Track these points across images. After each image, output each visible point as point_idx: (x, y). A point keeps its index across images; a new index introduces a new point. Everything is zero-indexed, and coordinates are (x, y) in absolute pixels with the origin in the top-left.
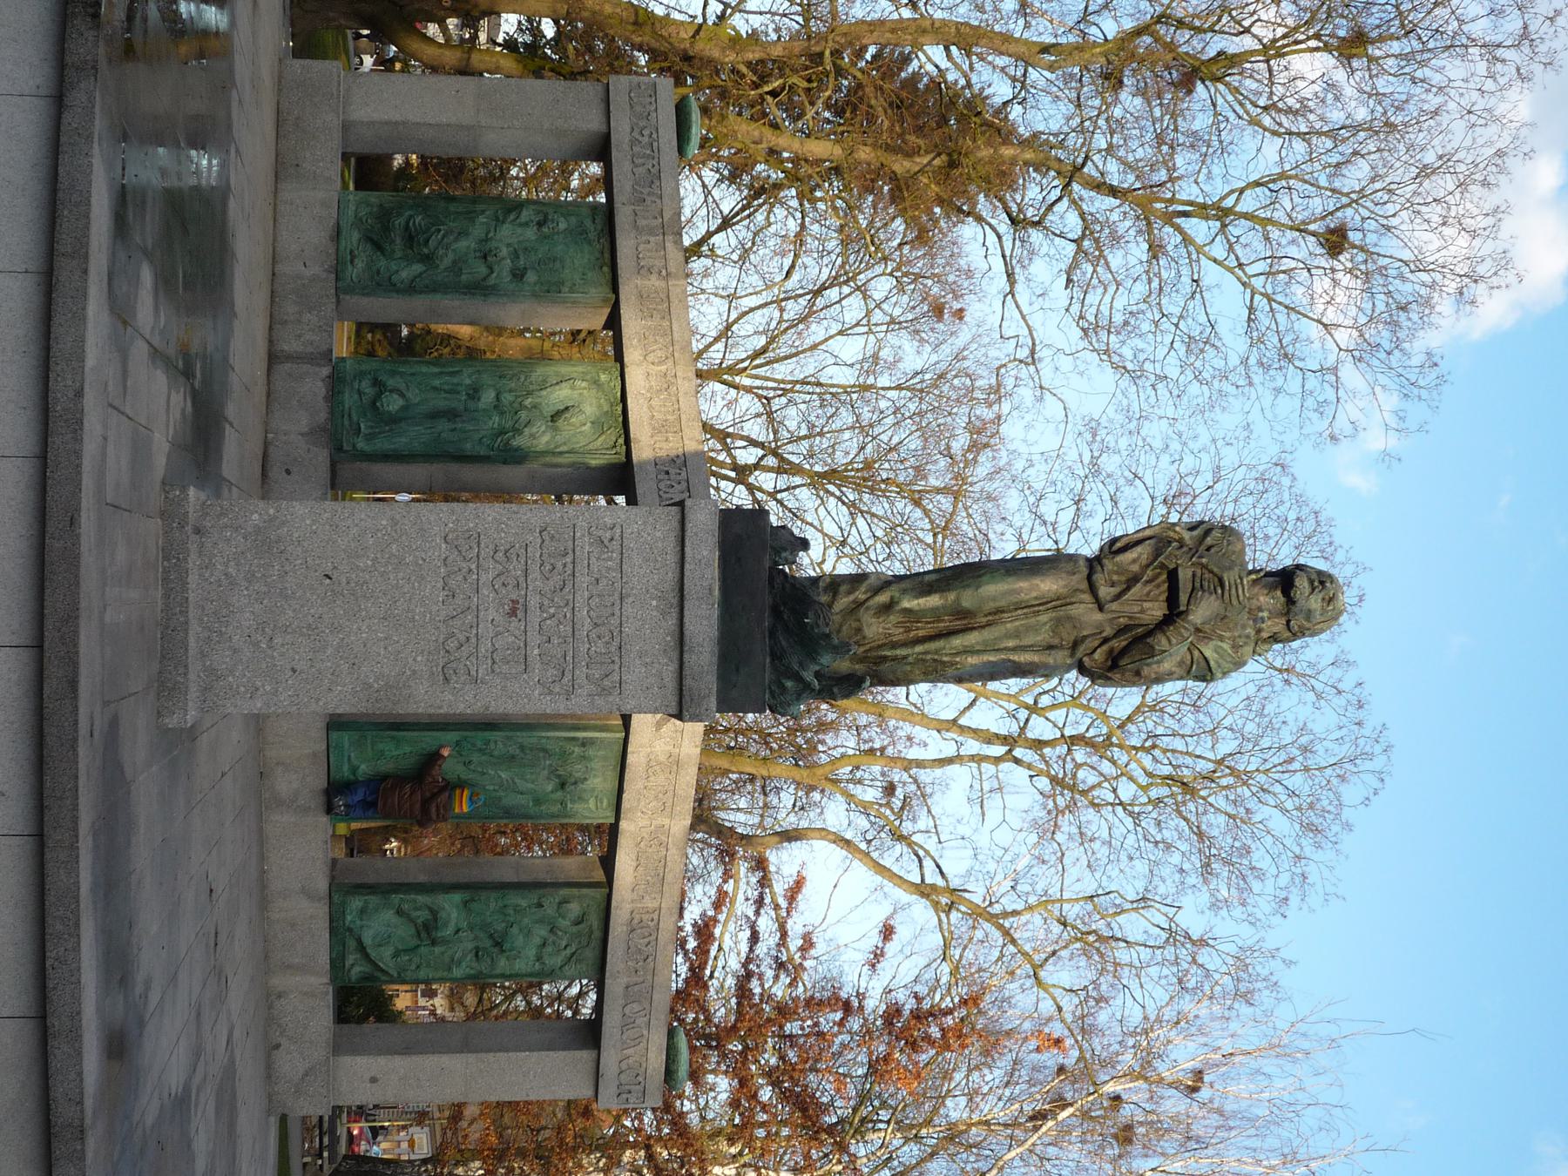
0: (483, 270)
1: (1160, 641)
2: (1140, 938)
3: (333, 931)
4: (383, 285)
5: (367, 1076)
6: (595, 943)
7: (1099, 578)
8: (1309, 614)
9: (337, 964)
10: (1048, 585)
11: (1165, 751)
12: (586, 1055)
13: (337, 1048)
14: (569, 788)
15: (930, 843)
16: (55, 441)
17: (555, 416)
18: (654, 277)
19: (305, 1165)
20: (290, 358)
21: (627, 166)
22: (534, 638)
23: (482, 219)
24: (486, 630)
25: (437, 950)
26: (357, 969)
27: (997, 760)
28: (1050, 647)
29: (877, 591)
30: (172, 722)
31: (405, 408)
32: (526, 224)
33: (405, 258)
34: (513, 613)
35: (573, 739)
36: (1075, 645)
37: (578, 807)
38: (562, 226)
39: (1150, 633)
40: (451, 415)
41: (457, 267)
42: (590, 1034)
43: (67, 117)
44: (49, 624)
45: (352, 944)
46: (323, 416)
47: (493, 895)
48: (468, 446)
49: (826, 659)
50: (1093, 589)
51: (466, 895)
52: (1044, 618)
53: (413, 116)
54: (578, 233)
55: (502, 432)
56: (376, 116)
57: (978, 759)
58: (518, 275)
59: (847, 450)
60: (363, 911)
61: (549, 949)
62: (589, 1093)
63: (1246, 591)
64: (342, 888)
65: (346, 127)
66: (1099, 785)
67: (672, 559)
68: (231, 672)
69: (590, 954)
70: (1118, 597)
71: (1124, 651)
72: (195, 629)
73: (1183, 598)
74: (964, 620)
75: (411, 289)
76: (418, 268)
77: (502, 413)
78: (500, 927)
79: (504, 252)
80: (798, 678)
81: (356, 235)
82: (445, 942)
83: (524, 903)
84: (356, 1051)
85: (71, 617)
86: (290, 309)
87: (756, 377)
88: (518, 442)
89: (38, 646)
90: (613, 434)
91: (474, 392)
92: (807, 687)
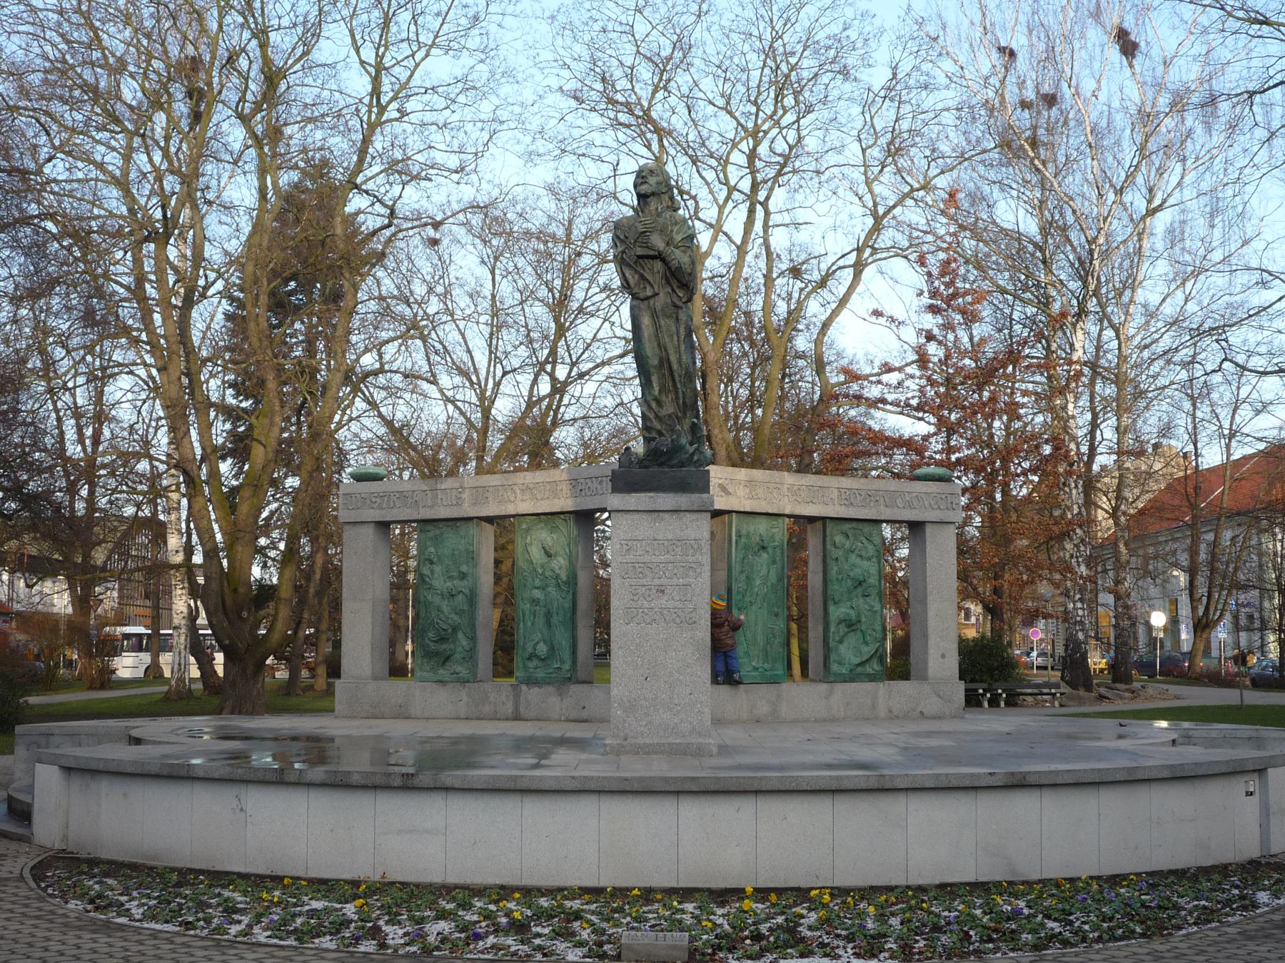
0: (460, 597)
1: (674, 264)
3: (852, 681)
4: (471, 655)
6: (860, 526)
7: (642, 295)
8: (659, 183)
9: (872, 678)
10: (646, 321)
11: (759, 93)
12: (929, 530)
13: (924, 677)
14: (766, 544)
16: (593, 787)
17: (549, 555)
18: (463, 496)
19: (1061, 706)
20: (516, 708)
21: (395, 511)
22: (675, 581)
23: (429, 598)
24: (671, 604)
25: (863, 620)
26: (876, 667)
27: (767, 214)
28: (677, 319)
29: (650, 407)
30: (715, 750)
31: (545, 642)
32: (432, 571)
33: (454, 642)
34: (663, 591)
36: (676, 306)
37: (777, 538)
38: (432, 550)
39: (669, 268)
40: (548, 615)
41: (460, 613)
42: (916, 528)
43: (457, 786)
44: (668, 789)
45: (860, 670)
46: (550, 689)
47: (830, 587)
48: (566, 605)
49: (684, 441)
50: (648, 298)
51: (830, 602)
52: (663, 323)
54: (437, 541)
55: (558, 585)
57: (766, 226)
58: (463, 576)
59: (539, 313)
60: (840, 663)
61: (863, 553)
62: (952, 526)
63: (649, 220)
64: (827, 676)
65: (375, 678)
66: (785, 138)
67: (636, 516)
69: (867, 528)
70: (651, 285)
71: (679, 281)
72: (671, 740)
73: (652, 253)
74: (665, 362)
75: (473, 639)
76: (460, 635)
77: (547, 586)
78: (850, 582)
79: (449, 584)
80: (693, 454)
81: (441, 671)
82: (859, 615)
83: (835, 568)
84: (925, 668)
85: (666, 780)
86: (487, 709)
87: (487, 380)
88: (564, 576)
89: (678, 793)
90: (559, 521)
91: (535, 602)
92: (697, 449)
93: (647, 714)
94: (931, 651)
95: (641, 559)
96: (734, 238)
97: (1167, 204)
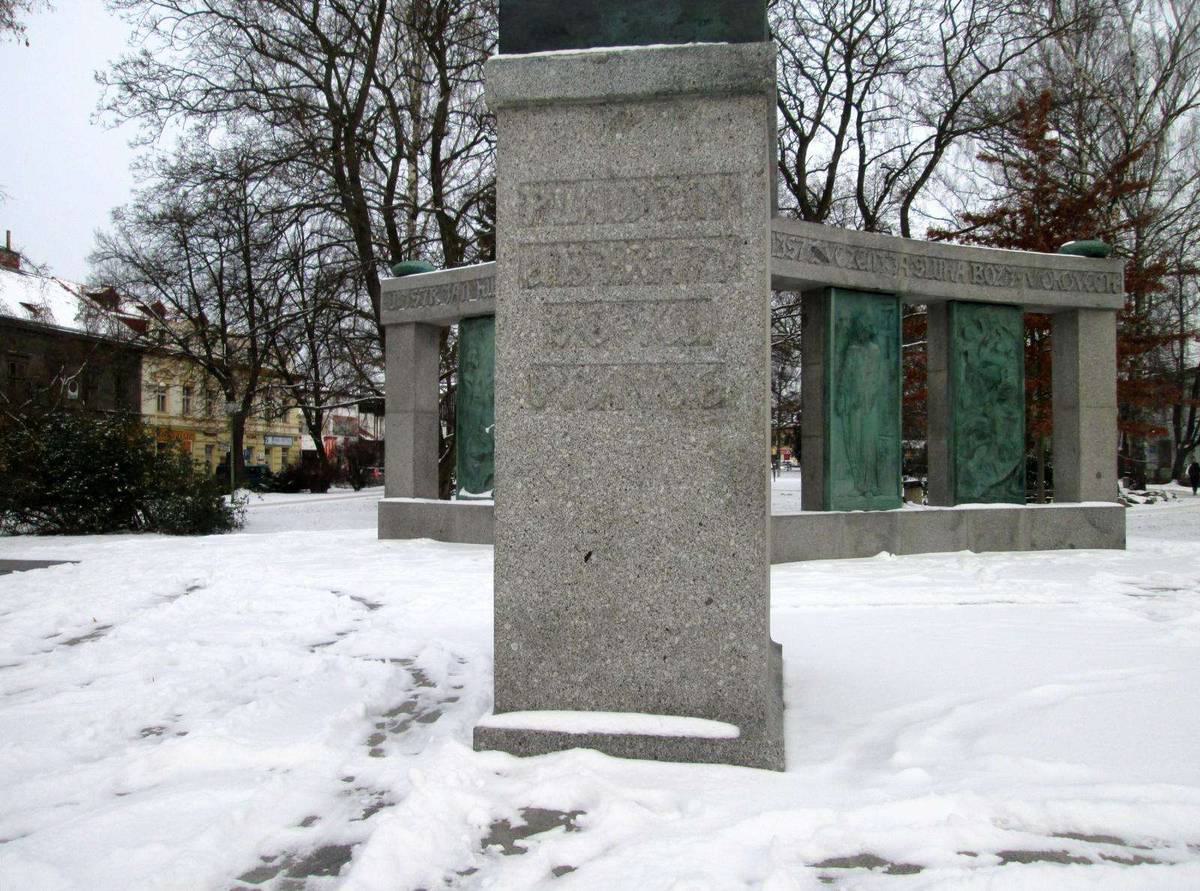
2: (969, 12)
5: (1096, 480)
12: (1082, 320)
15: (909, 150)
22: (663, 292)
27: (860, 114)
35: (836, 327)
53: (410, 453)
56: (411, 476)
57: (859, 124)
68: (712, 682)
93: (590, 655)
94: (1084, 470)
95: (574, 234)
96: (833, 130)
97: (1192, 104)
